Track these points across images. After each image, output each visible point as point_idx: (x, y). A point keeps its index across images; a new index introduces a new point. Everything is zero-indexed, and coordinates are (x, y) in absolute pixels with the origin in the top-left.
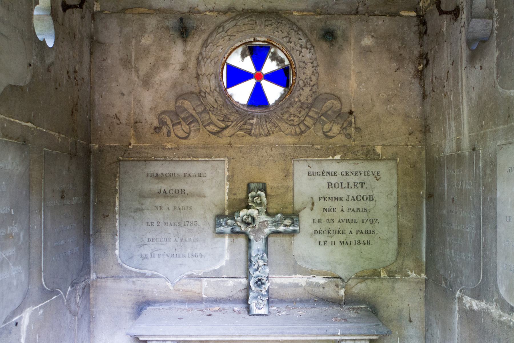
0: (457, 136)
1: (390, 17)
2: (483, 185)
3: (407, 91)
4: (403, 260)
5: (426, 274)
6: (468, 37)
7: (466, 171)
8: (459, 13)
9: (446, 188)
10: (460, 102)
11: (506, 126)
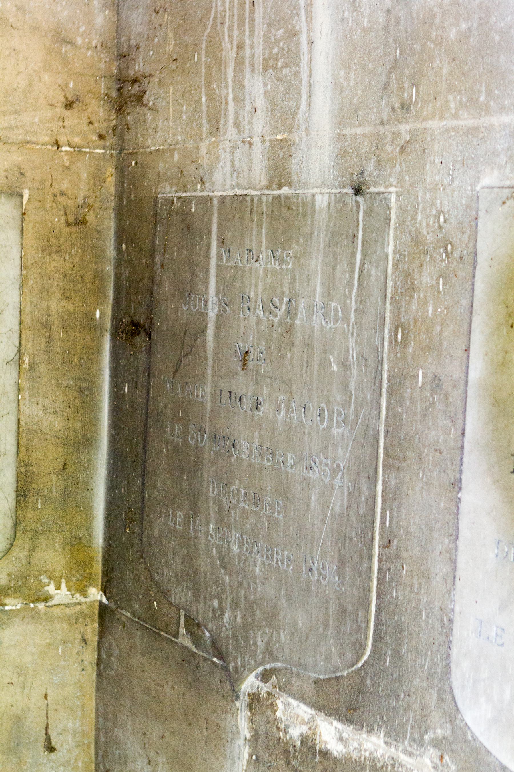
0: (276, 130)
2: (398, 325)
4: (33, 548)
5: (104, 590)
7: (316, 263)
9: (212, 314)
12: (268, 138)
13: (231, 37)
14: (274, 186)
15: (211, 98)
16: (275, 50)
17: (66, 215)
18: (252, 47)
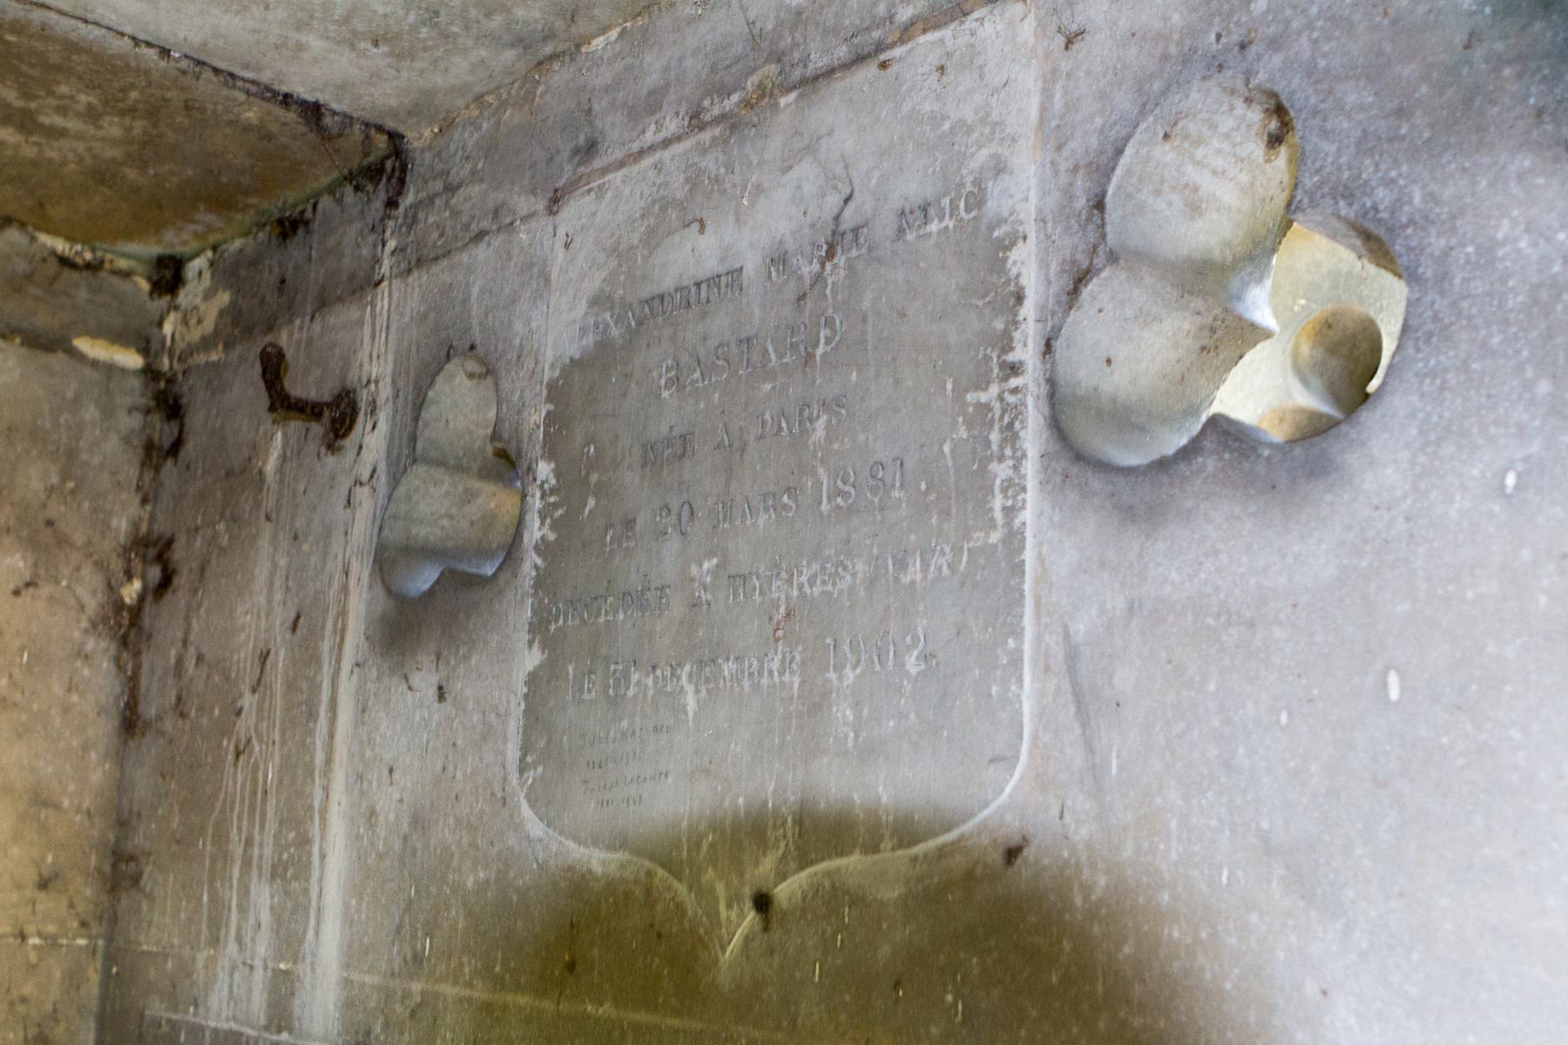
0: (282, 958)
1: (24, 351)
3: (58, 690)
6: (386, 533)
8: (353, 421)
10: (310, 808)
11: (548, 1005)
12: (270, 964)
13: (240, 828)
14: (274, 1029)
15: (214, 898)
16: (285, 856)
17: (25, 1028)
18: (261, 845)
